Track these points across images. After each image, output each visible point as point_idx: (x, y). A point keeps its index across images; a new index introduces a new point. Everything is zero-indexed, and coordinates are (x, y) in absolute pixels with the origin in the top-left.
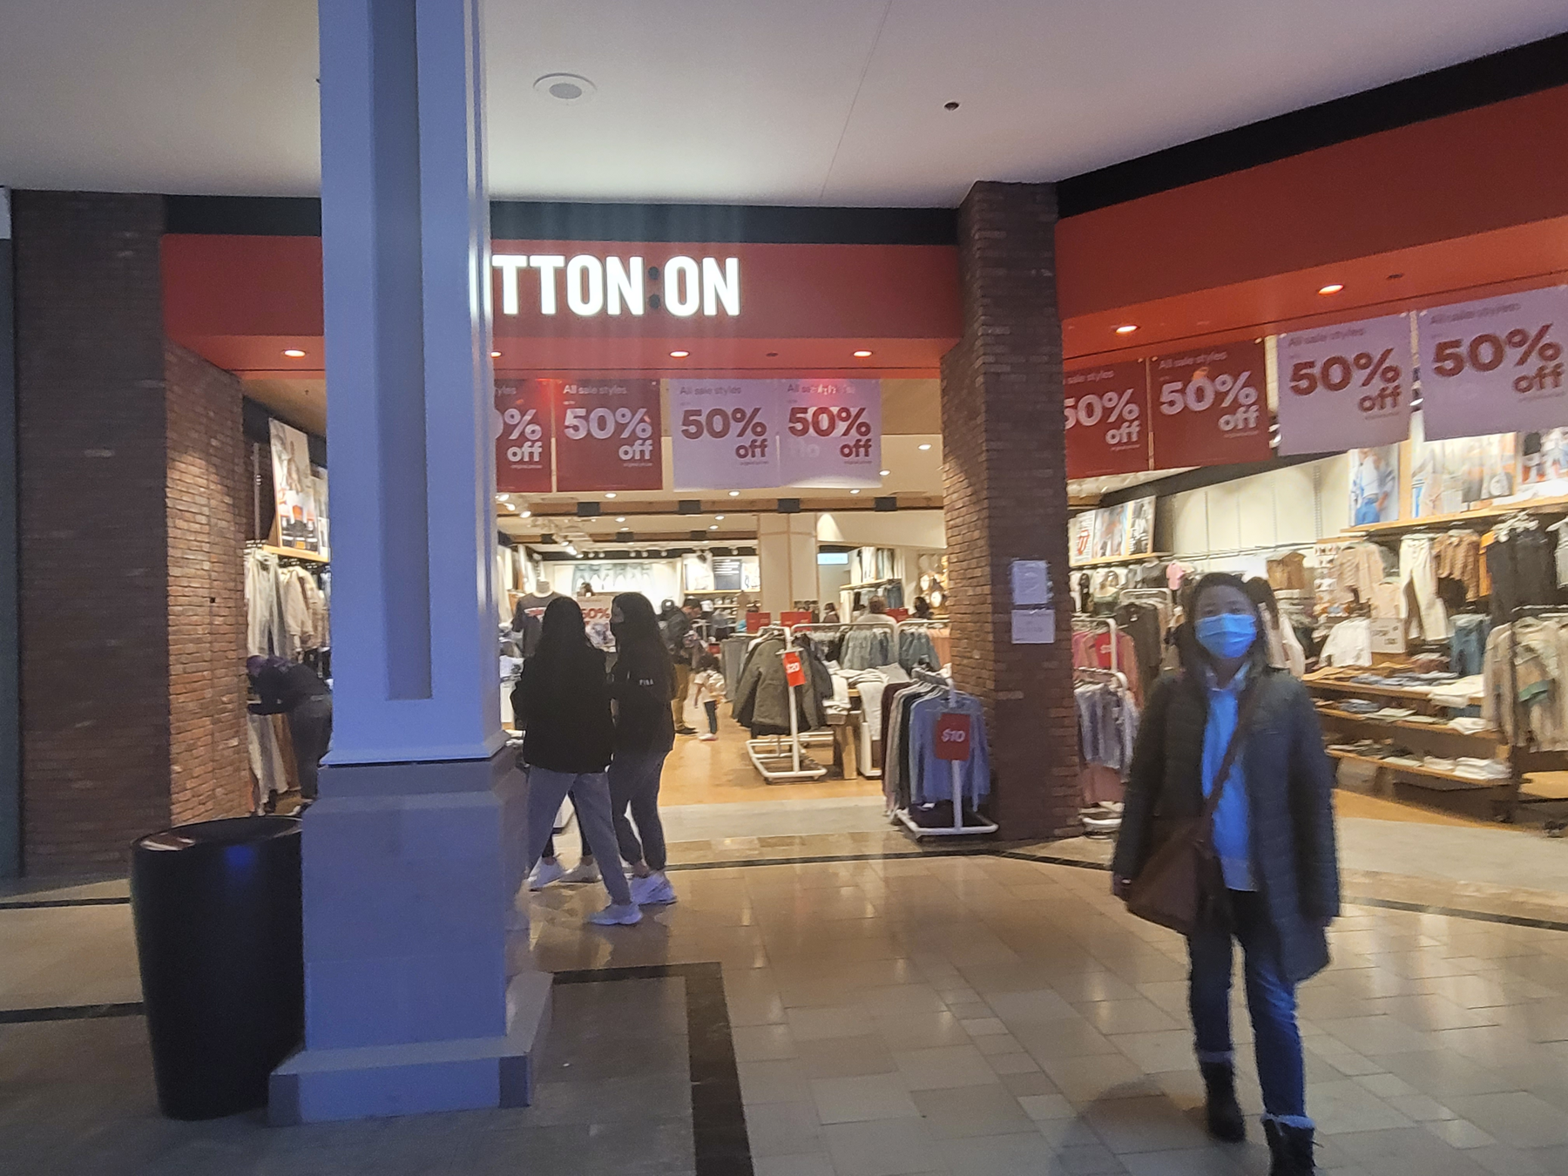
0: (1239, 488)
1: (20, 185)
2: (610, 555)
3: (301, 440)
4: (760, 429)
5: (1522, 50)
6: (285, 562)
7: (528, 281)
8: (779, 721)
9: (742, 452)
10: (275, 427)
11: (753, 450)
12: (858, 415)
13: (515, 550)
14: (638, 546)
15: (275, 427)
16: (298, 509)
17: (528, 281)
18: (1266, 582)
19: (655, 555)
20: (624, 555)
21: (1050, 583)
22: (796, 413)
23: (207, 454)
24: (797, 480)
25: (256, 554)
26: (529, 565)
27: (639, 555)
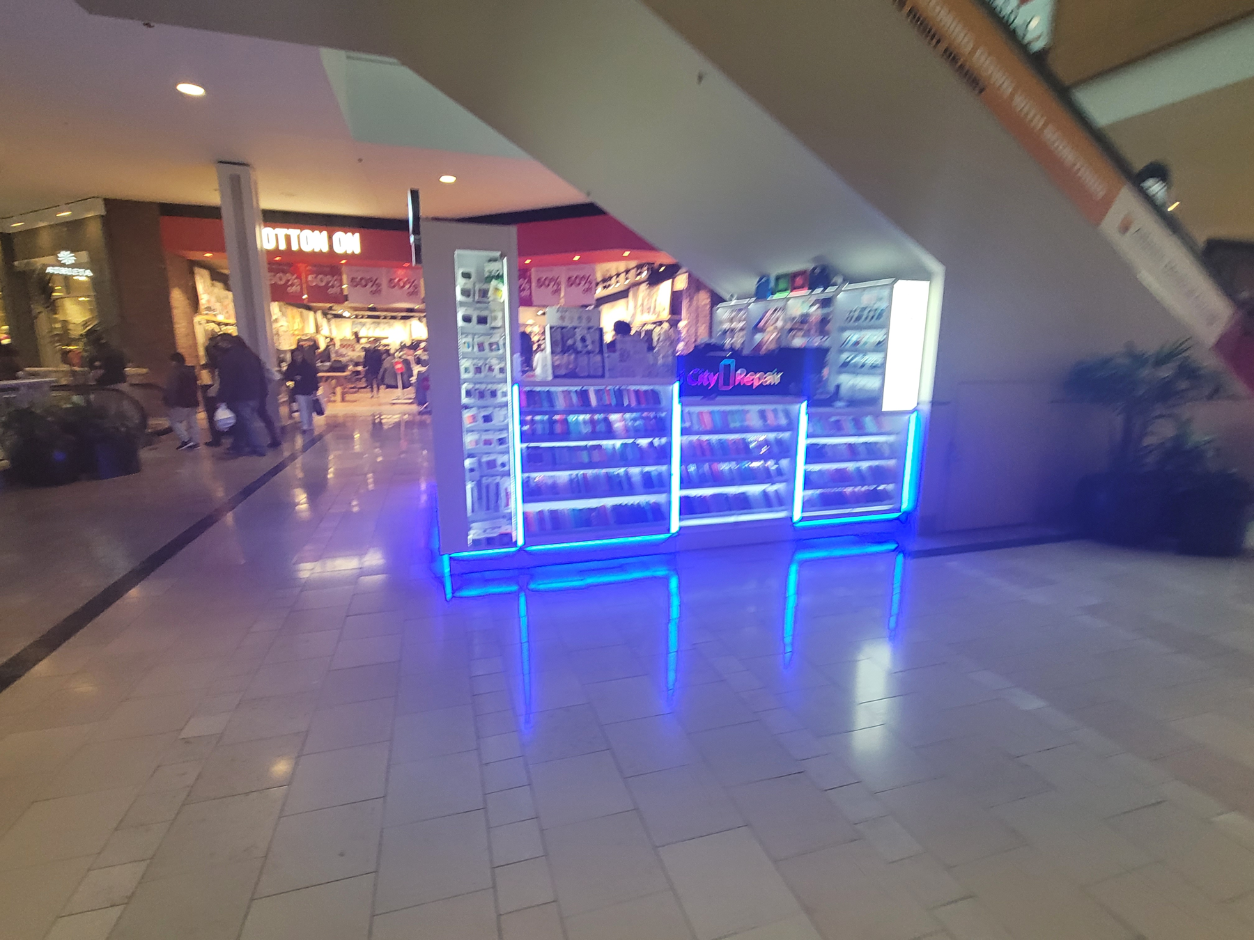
0: (613, 306)
1: (111, 196)
2: (369, 317)
3: (206, 273)
4: (379, 285)
5: (550, 209)
6: (208, 322)
7: (288, 238)
8: (394, 384)
9: (373, 293)
10: (197, 270)
11: (377, 292)
12: (413, 282)
13: (315, 312)
14: (385, 313)
15: (197, 270)
16: (208, 301)
17: (288, 238)
18: (237, 340)
19: (394, 318)
20: (378, 317)
21: (103, 341)
22: (391, 280)
23: (180, 287)
24: (395, 302)
25: (197, 319)
26: (325, 320)
27: (385, 318)
